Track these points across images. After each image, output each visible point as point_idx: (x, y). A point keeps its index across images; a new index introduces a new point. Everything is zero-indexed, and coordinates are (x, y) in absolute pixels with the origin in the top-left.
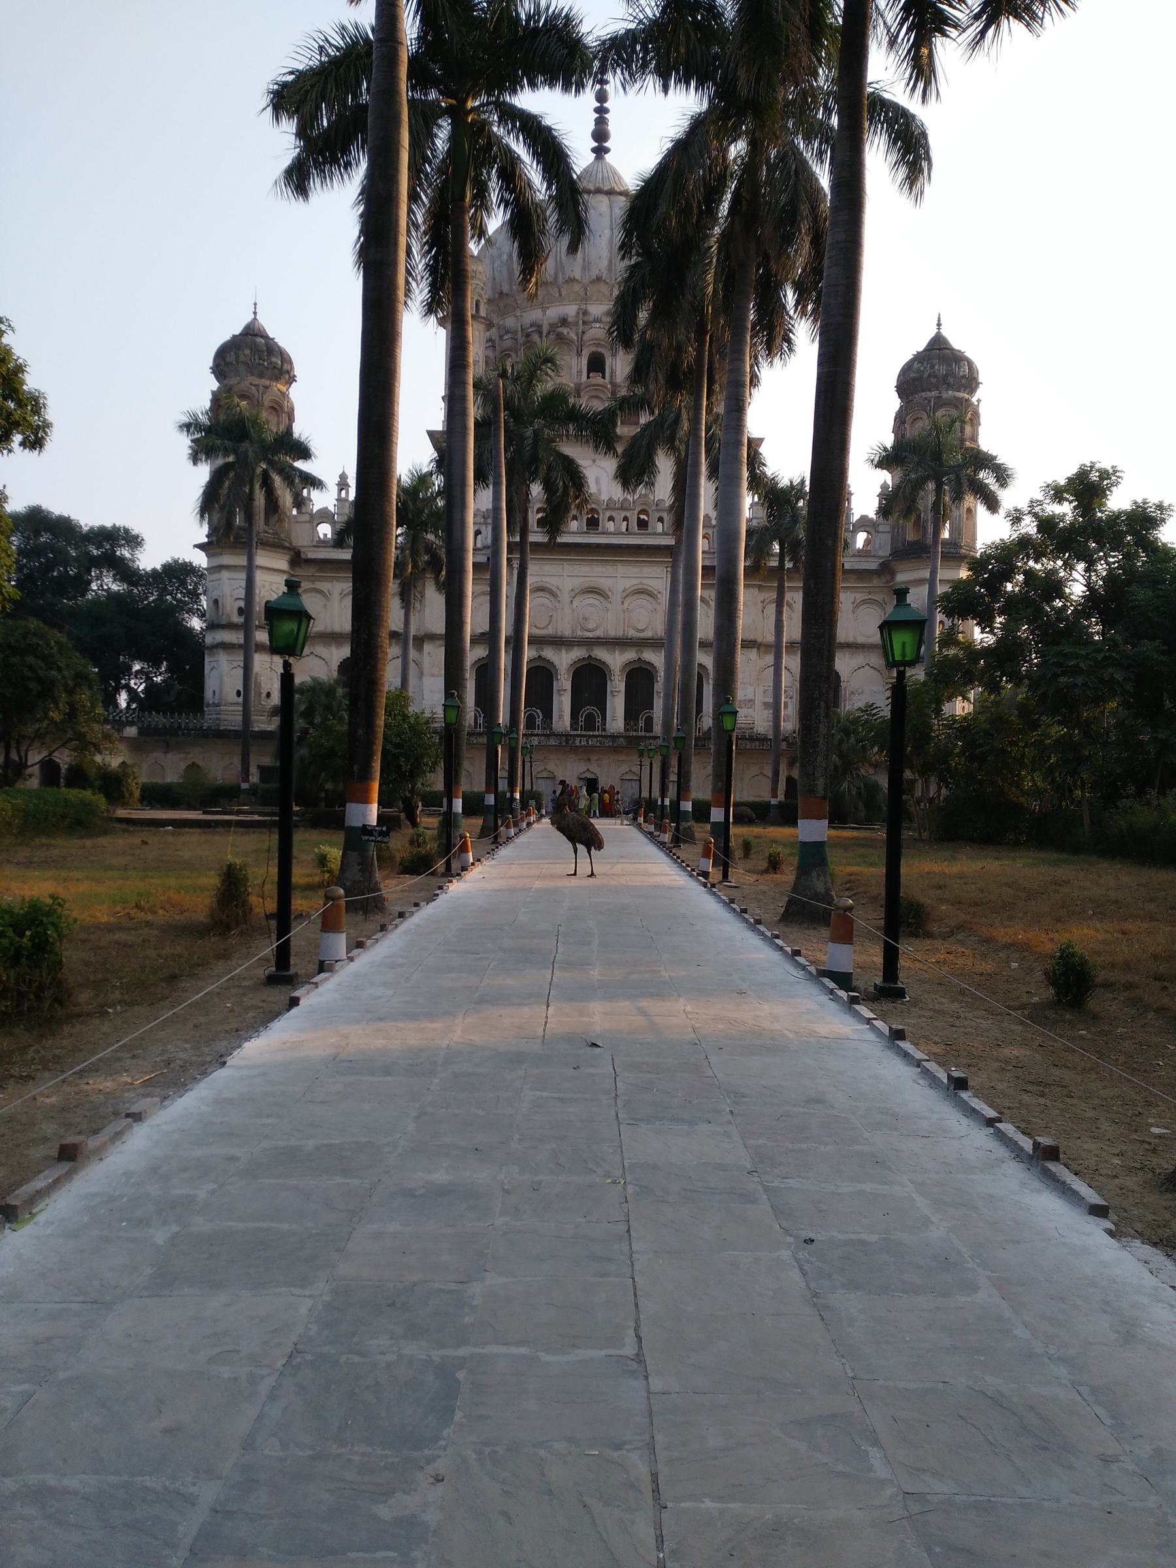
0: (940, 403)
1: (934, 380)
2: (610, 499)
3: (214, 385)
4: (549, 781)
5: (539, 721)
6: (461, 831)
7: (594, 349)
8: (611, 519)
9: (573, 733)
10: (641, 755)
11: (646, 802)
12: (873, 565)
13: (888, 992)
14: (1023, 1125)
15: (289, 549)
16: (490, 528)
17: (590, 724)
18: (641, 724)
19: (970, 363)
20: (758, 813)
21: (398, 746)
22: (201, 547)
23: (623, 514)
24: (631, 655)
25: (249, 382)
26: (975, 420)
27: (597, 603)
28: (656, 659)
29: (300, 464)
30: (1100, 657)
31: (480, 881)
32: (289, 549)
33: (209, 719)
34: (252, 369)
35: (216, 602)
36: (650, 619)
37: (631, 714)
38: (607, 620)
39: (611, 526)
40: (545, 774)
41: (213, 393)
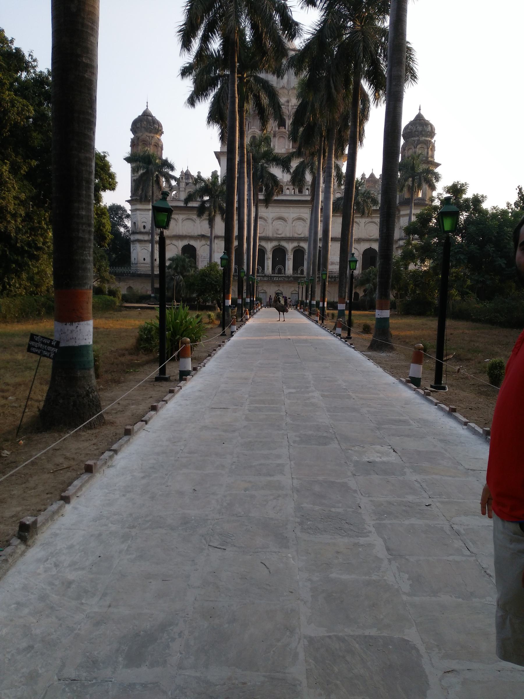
0: (419, 142)
1: (417, 133)
3: (132, 136)
4: (264, 294)
5: (260, 271)
8: (288, 189)
9: (273, 275)
10: (299, 284)
13: (349, 338)
14: (136, 141)
17: (280, 272)
18: (299, 272)
19: (431, 126)
21: (216, 282)
22: (128, 201)
24: (295, 244)
25: (145, 135)
26: (433, 149)
27: (282, 223)
28: (304, 245)
29: (171, 173)
30: (456, 251)
31: (251, 322)
33: (133, 269)
34: (147, 130)
35: (135, 223)
36: (302, 230)
37: (295, 268)
38: (286, 230)
39: (288, 192)
40: (262, 291)
41: (132, 139)
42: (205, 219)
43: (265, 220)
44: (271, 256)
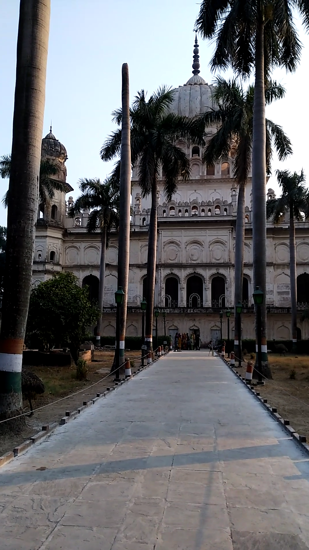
6: (124, 358)
8: (203, 211)
10: (221, 317)
16: (149, 216)
20: (276, 348)
23: (209, 208)
24: (214, 271)
37: (215, 297)
40: (173, 328)
44: (185, 286)
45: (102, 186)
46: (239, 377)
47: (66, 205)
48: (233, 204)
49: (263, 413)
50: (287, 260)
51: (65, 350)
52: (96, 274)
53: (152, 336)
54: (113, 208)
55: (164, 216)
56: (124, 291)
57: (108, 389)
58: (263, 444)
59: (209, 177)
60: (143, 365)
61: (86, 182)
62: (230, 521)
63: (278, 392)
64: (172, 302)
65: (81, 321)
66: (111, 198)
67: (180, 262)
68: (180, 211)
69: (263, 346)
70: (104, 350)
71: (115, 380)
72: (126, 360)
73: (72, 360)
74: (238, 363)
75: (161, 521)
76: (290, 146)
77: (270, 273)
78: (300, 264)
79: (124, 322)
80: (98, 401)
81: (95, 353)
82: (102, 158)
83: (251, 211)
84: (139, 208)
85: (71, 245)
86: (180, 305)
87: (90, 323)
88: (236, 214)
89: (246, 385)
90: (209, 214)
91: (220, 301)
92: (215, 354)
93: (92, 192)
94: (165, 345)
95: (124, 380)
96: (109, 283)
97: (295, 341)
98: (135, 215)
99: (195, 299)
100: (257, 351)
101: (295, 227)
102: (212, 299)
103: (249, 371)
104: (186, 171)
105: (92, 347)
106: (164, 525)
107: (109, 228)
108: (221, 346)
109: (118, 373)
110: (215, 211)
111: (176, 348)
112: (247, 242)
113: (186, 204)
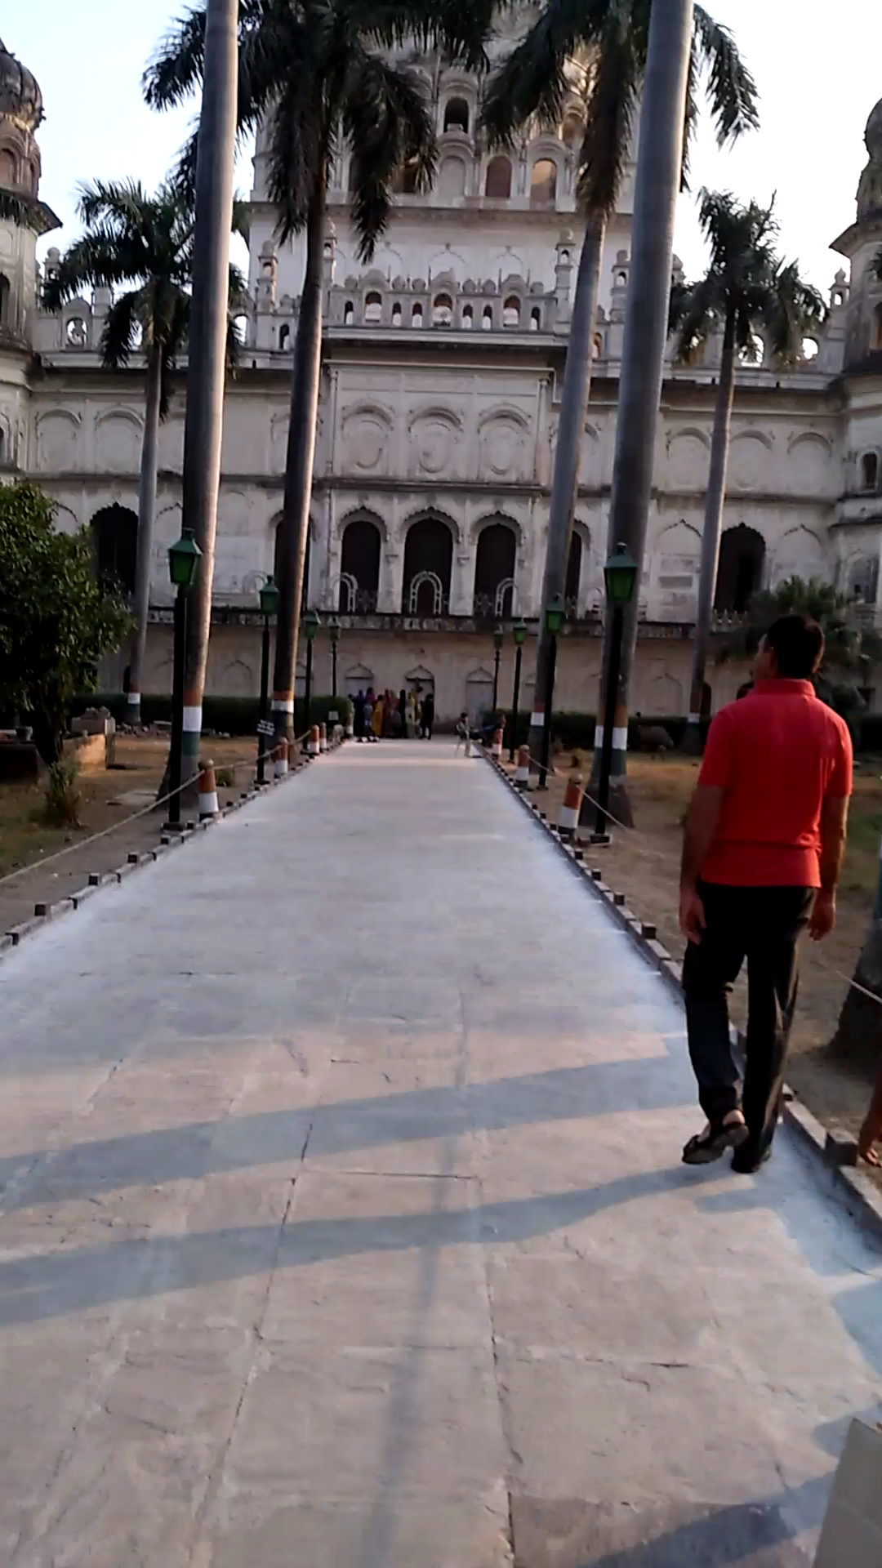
2: (469, 281)
6: (198, 758)
7: (454, 94)
8: (468, 311)
10: (499, 643)
11: (508, 716)
12: (819, 384)
15: (23, 352)
24: (486, 507)
32: (23, 352)
40: (358, 673)
42: (177, 416)
43: (384, 417)
44: (400, 549)
45: (148, 209)
46: (539, 821)
47: (38, 276)
48: (560, 295)
49: (614, 936)
50: (702, 481)
51: (22, 734)
52: (130, 501)
53: (292, 694)
54: (184, 283)
55: (349, 321)
56: (203, 546)
57: (133, 859)
58: (619, 1055)
59: (492, 204)
60: (261, 780)
61: (98, 193)
62: (508, 1436)
63: (649, 866)
64: (359, 595)
65: (66, 642)
66: (180, 246)
67: (391, 474)
68: (397, 308)
69: (616, 731)
70: (150, 735)
71: (166, 827)
72: (201, 766)
73: (40, 762)
74: (537, 777)
75: (220, 1464)
76: (754, 101)
77: (655, 518)
78: (735, 499)
79: (199, 646)
80: (93, 898)
81: (117, 743)
82: (148, 99)
83: (608, 324)
84: (269, 290)
85: (52, 406)
86: (382, 606)
87: (97, 651)
88: (566, 330)
89: (559, 846)
90: (486, 323)
91: (499, 598)
92: (474, 751)
93: (117, 227)
94: (331, 724)
95: (191, 826)
96: (164, 530)
97: (693, 718)
98: (256, 315)
99: (426, 590)
100: (598, 742)
101: (735, 382)
102: (476, 592)
103: (570, 802)
104: (423, 157)
105: (109, 725)
106: (230, 1487)
107: (170, 350)
108: (498, 730)
109: (178, 805)
110: (505, 318)
111: (361, 732)
112: (591, 420)
113: (418, 288)
